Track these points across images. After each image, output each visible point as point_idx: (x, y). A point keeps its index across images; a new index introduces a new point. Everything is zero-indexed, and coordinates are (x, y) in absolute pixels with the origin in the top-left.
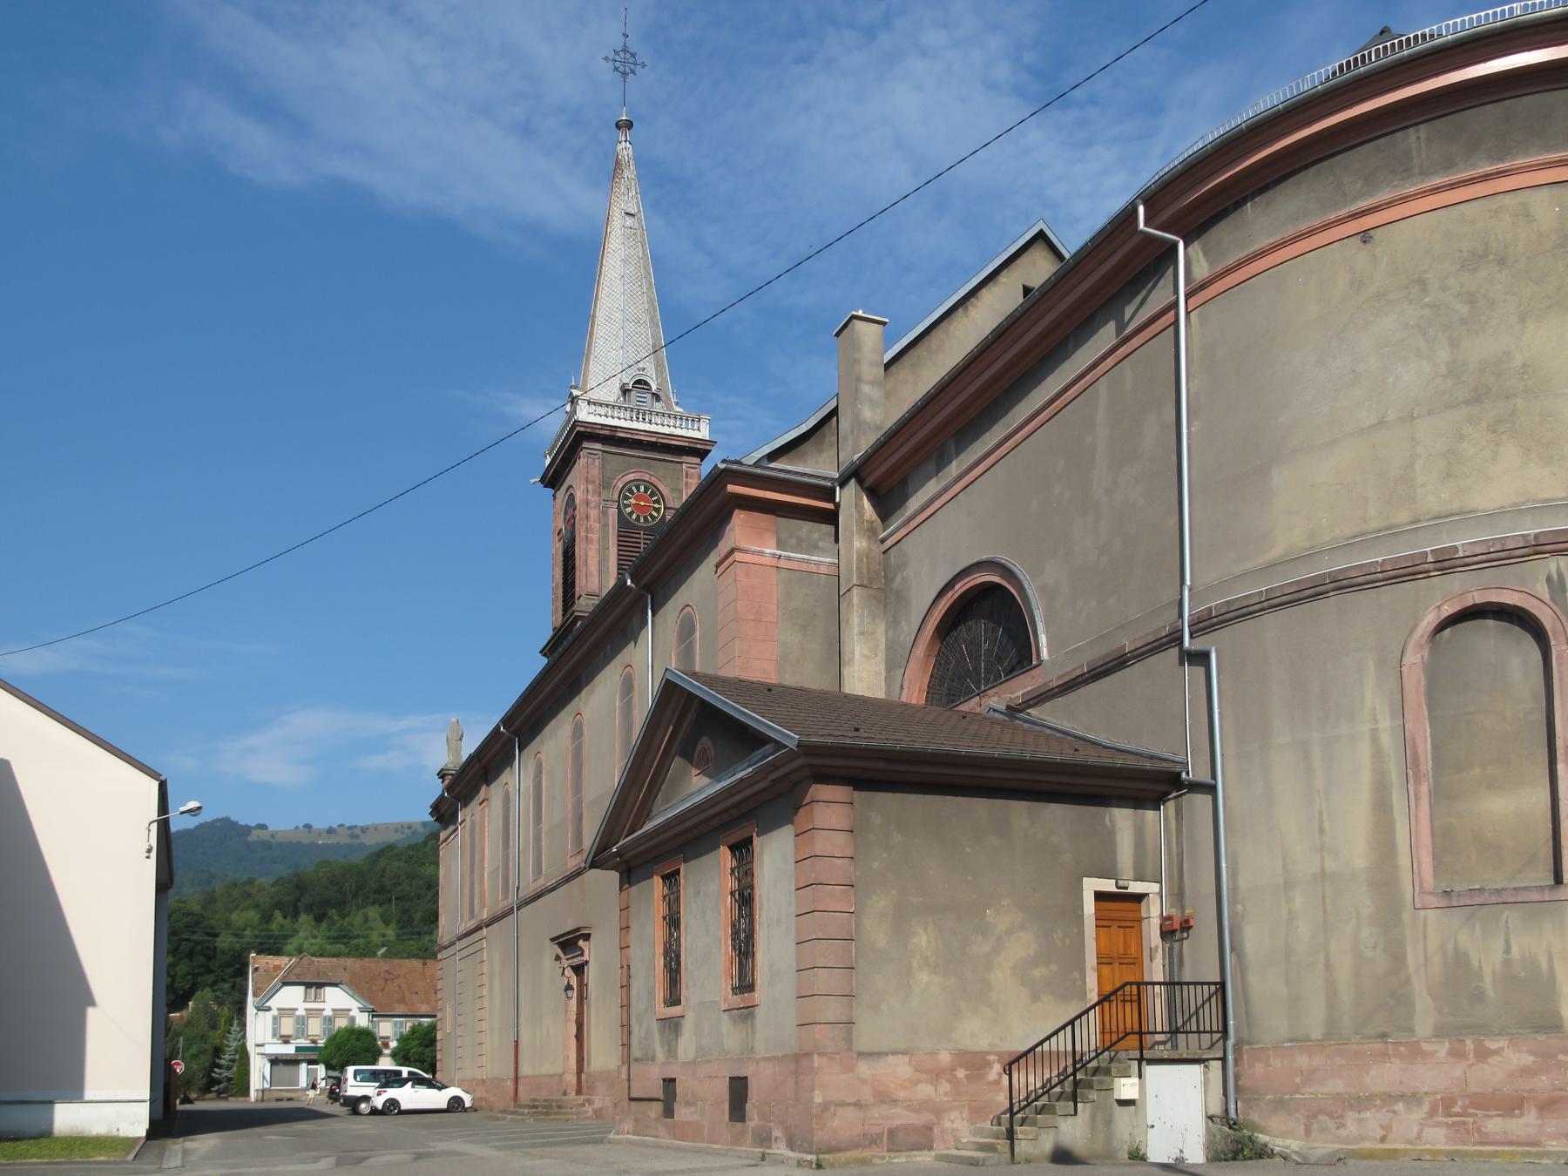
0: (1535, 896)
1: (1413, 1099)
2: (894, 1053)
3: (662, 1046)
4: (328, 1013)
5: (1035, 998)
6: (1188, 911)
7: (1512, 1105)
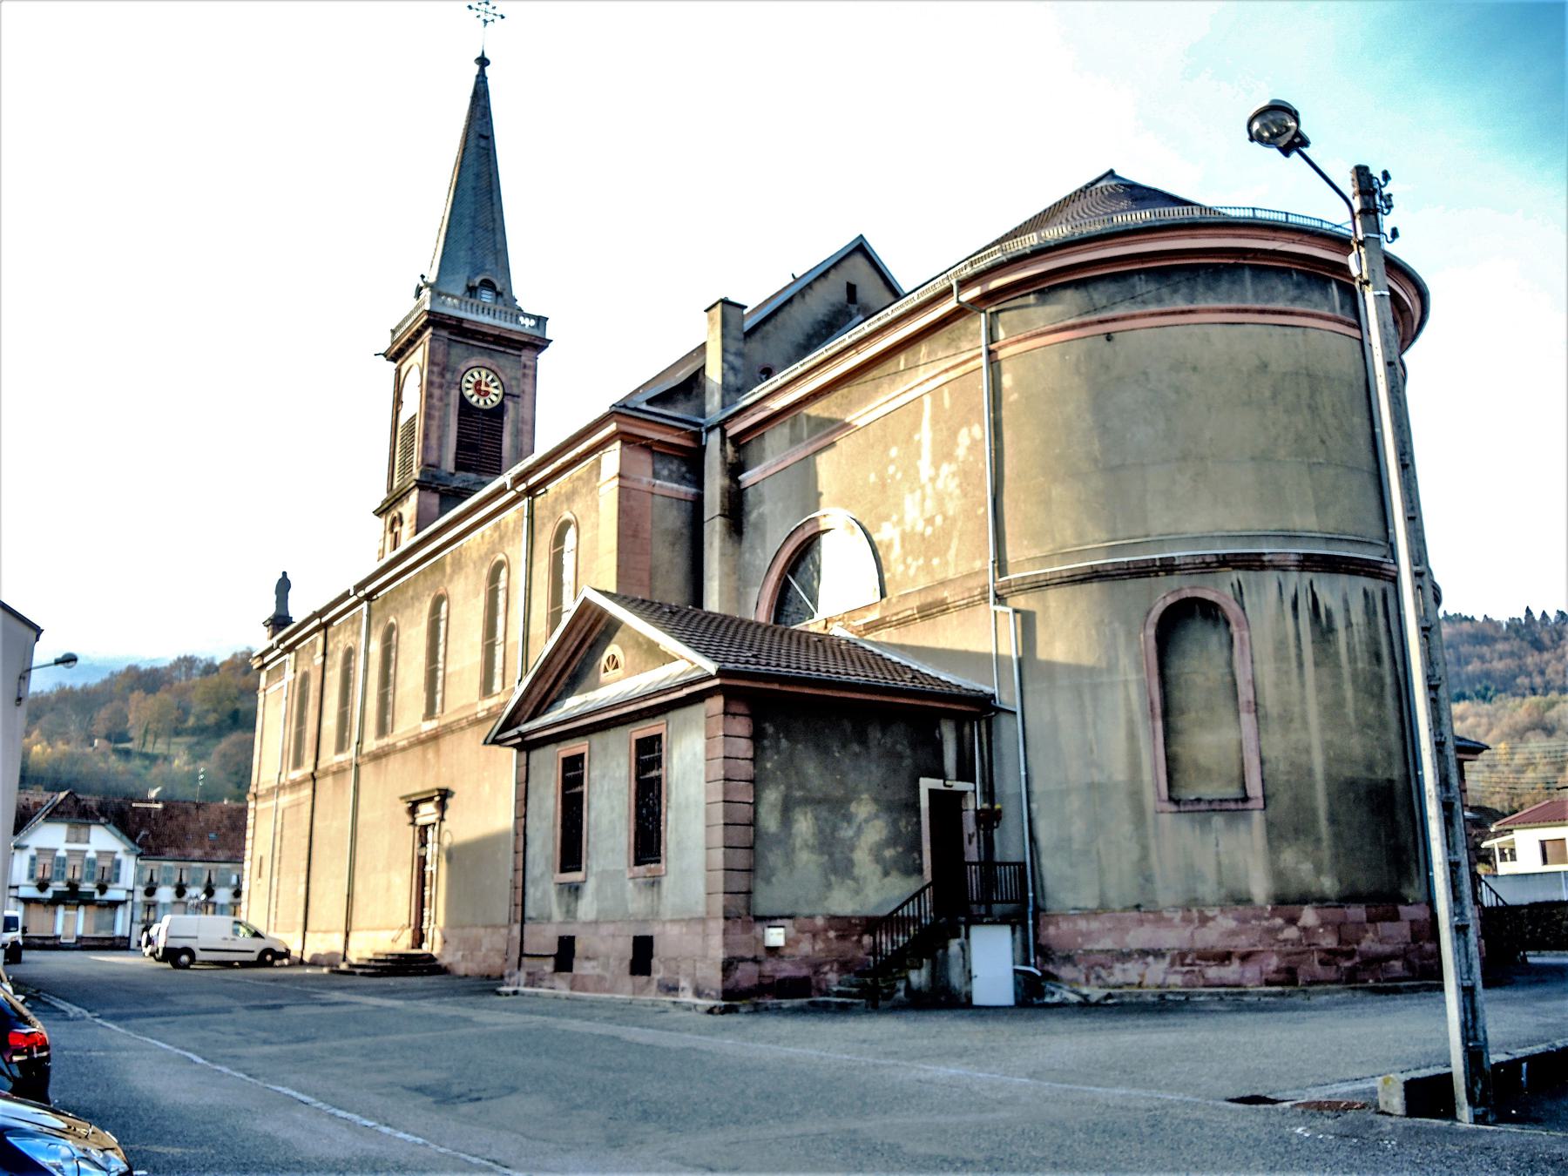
0: (1232, 806)
1: (1158, 954)
2: (782, 917)
3: (560, 905)
4: (91, 855)
5: (886, 874)
6: (997, 806)
7: (1224, 958)
